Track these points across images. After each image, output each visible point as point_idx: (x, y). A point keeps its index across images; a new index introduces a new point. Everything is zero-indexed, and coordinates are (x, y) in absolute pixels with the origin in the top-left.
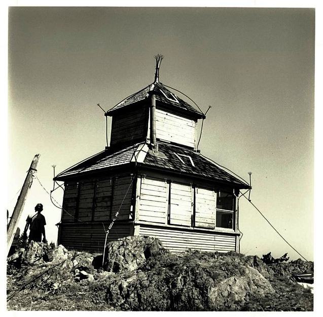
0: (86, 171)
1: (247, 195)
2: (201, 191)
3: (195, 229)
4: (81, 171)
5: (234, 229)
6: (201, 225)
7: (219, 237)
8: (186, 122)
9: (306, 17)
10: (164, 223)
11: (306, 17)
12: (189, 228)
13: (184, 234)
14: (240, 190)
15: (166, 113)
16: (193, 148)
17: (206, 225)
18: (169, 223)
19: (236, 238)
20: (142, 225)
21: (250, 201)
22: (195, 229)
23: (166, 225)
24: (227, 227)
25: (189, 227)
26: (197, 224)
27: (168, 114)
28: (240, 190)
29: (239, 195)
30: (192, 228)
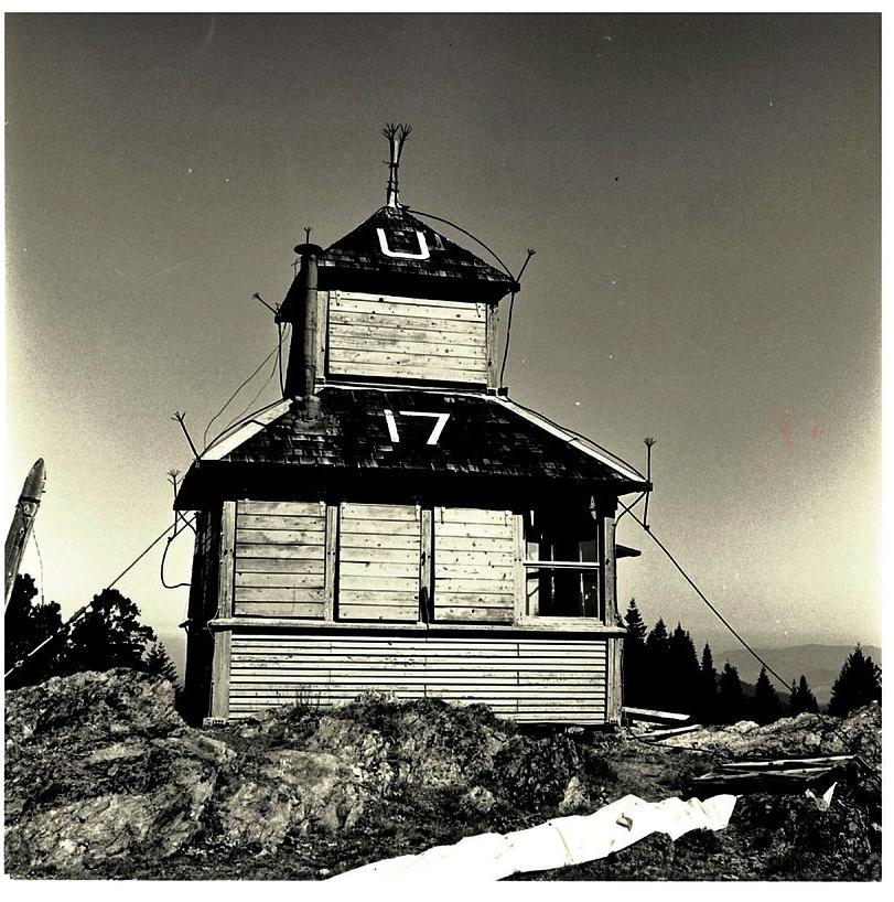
0: (343, 387)
1: (638, 510)
2: (348, 509)
3: (432, 626)
4: (11, 590)
5: (603, 619)
6: (458, 613)
7: (528, 646)
8: (451, 314)
9: (873, 21)
10: (323, 619)
11: (873, 21)
12: (413, 627)
13: (394, 645)
14: (620, 498)
15: (378, 297)
16: (484, 386)
17: (482, 614)
18: (336, 618)
19: (607, 645)
20: (238, 629)
21: (647, 528)
22: (432, 626)
23: (330, 622)
24: (576, 613)
25: (414, 622)
26: (439, 614)
27: (388, 298)
28: (620, 498)
29: (617, 514)
30: (422, 626)
